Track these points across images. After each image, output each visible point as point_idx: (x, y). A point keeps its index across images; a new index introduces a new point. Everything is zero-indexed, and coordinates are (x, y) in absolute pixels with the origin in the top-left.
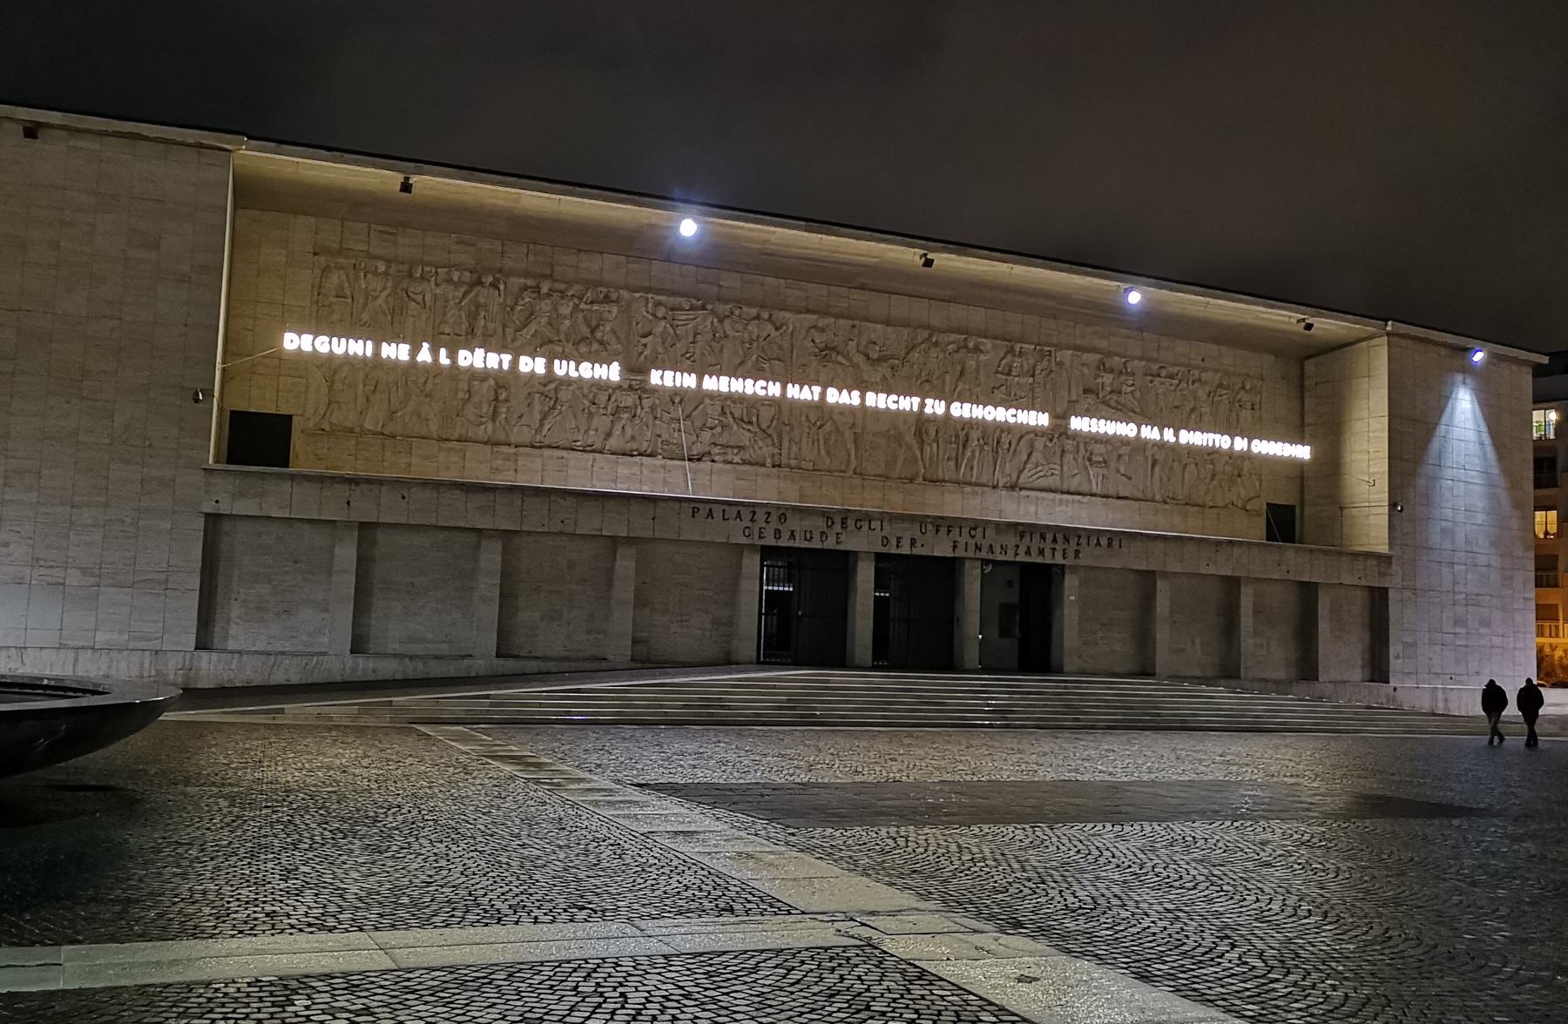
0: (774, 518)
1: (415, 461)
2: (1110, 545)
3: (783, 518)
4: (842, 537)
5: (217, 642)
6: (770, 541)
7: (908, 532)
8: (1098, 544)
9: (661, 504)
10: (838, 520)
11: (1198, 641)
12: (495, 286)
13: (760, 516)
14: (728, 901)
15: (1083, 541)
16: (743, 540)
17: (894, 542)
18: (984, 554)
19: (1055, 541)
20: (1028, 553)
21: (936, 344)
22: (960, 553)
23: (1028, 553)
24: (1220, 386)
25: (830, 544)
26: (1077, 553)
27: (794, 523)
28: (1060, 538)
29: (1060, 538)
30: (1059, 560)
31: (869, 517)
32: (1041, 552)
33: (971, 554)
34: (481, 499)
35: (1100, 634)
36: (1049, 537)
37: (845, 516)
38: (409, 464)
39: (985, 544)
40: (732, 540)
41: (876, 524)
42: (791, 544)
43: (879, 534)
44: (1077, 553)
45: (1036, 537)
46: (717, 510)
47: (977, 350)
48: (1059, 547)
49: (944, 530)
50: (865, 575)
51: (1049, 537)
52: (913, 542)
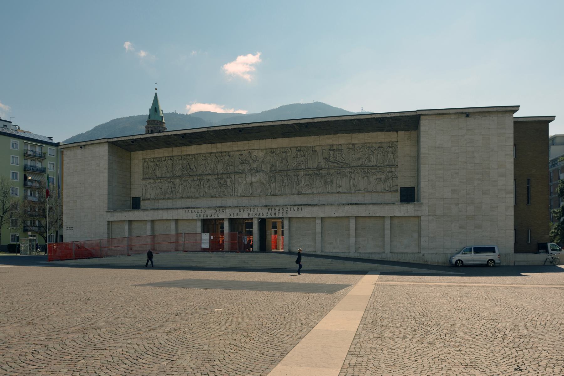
2: (298, 210)
6: (202, 218)
9: (179, 210)
12: (171, 160)
15: (289, 209)
18: (257, 216)
19: (279, 210)
20: (271, 215)
21: (273, 153)
22: (250, 217)
23: (271, 215)
24: (379, 147)
25: (216, 217)
26: (287, 213)
28: (281, 209)
29: (281, 209)
32: (275, 214)
39: (258, 213)
43: (228, 213)
48: (281, 212)
50: (226, 225)
51: (277, 209)
52: (237, 215)
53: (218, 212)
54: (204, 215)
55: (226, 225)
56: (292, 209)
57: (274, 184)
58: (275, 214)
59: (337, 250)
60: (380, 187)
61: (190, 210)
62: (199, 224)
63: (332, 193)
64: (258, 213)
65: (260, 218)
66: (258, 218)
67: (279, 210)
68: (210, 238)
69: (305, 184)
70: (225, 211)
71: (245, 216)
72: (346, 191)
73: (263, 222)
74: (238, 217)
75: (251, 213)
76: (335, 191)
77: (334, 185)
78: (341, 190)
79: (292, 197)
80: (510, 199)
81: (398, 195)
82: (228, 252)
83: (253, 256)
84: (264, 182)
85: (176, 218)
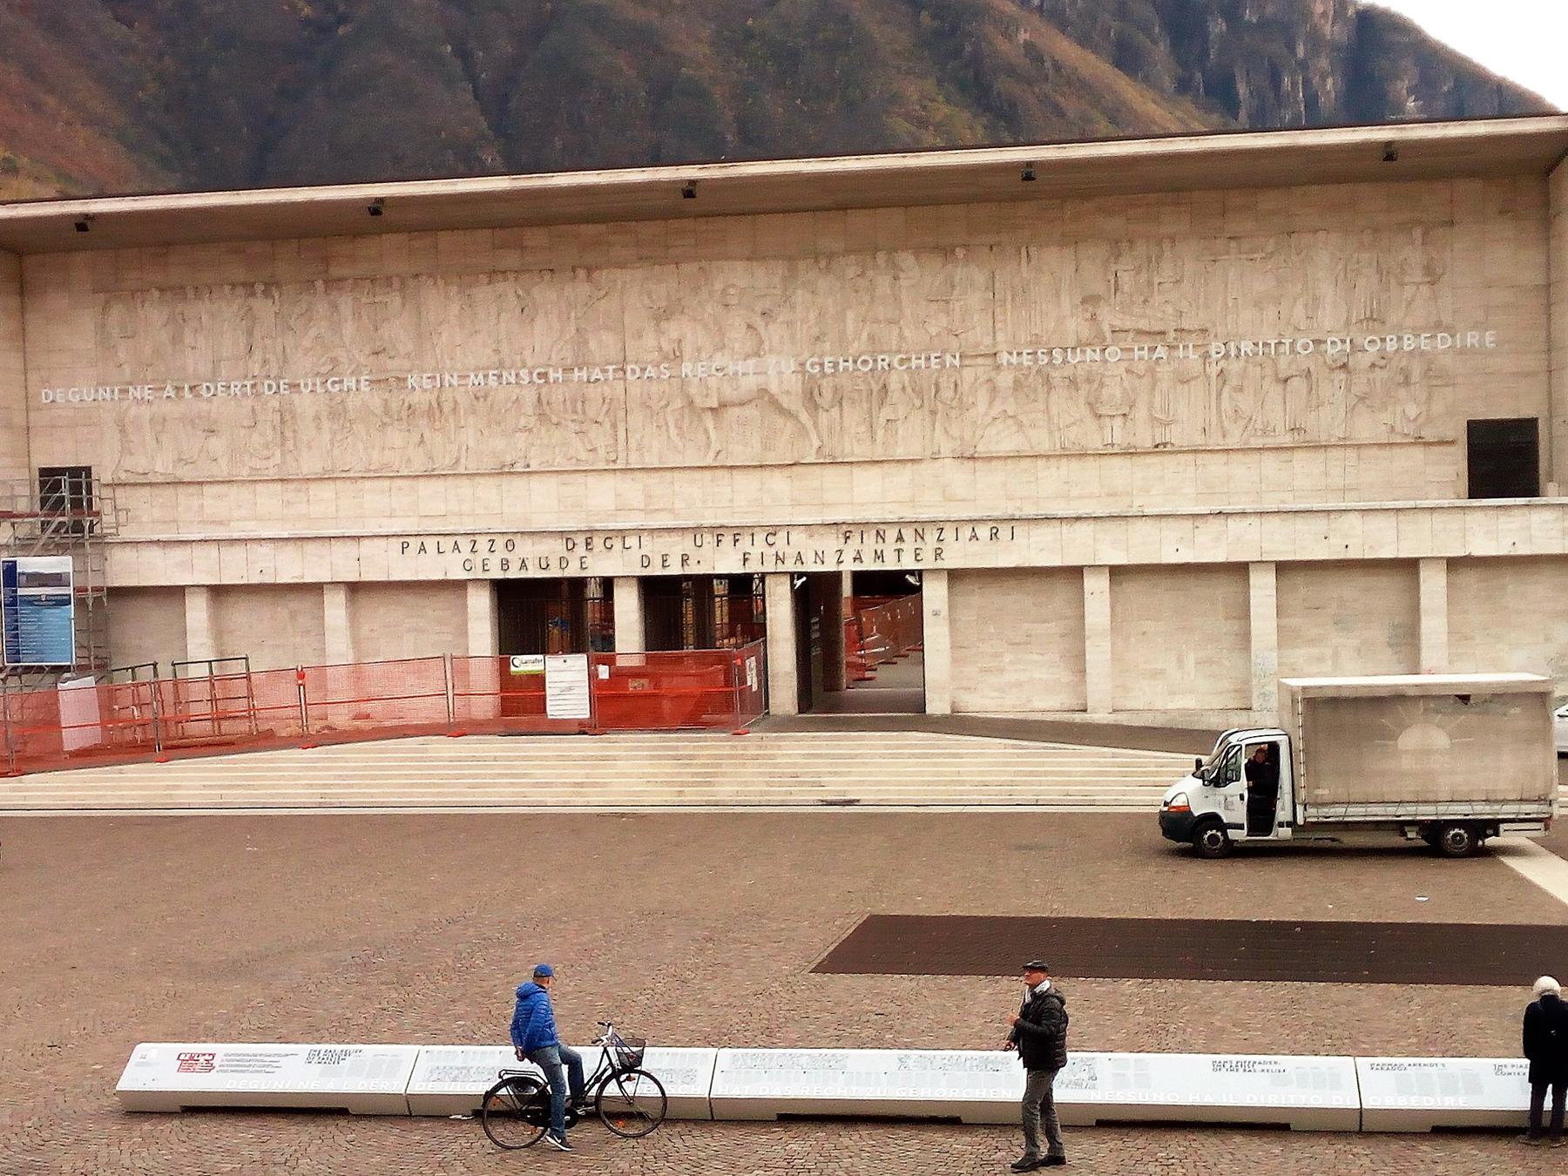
0: (500, 542)
1: (207, 502)
2: (994, 535)
3: (510, 545)
4: (588, 562)
5: (959, 587)
6: (497, 574)
7: (685, 544)
8: (975, 537)
9: (366, 542)
10: (580, 540)
11: (1191, 659)
13: (483, 544)
14: (861, 657)
15: (949, 534)
16: (463, 576)
17: (657, 561)
18: (790, 566)
19: (900, 538)
20: (858, 558)
22: (753, 567)
26: (938, 554)
27: (526, 548)
28: (908, 533)
29: (908, 533)
30: (908, 563)
31: (622, 533)
32: (879, 556)
33: (769, 567)
34: (179, 554)
35: (1008, 658)
36: (891, 534)
37: (589, 535)
38: (202, 506)
39: (791, 553)
40: (451, 577)
41: (632, 541)
42: (523, 575)
43: (635, 554)
44: (938, 554)
45: (870, 537)
46: (430, 543)
47: (607, 462)
48: (909, 546)
49: (727, 539)
51: (891, 534)
52: (685, 560)
53: (581, 550)
54: (505, 564)
55: (628, 609)
56: (968, 533)
57: (835, 412)
58: (879, 556)
59: (1188, 702)
60: (1367, 428)
61: (430, 543)
62: (481, 604)
63: (1130, 453)
64: (791, 553)
65: (800, 575)
66: (793, 576)
67: (900, 538)
68: (592, 676)
69: (995, 412)
70: (617, 543)
71: (725, 561)
72: (1199, 440)
73: (814, 594)
74: (689, 571)
75: (755, 552)
76: (1144, 440)
77: (1141, 413)
78: (1176, 436)
79: (926, 469)
80: (1525, 922)
81: (1455, 463)
82: (582, 728)
83: (1479, 808)
84: (785, 401)
85: (352, 577)
